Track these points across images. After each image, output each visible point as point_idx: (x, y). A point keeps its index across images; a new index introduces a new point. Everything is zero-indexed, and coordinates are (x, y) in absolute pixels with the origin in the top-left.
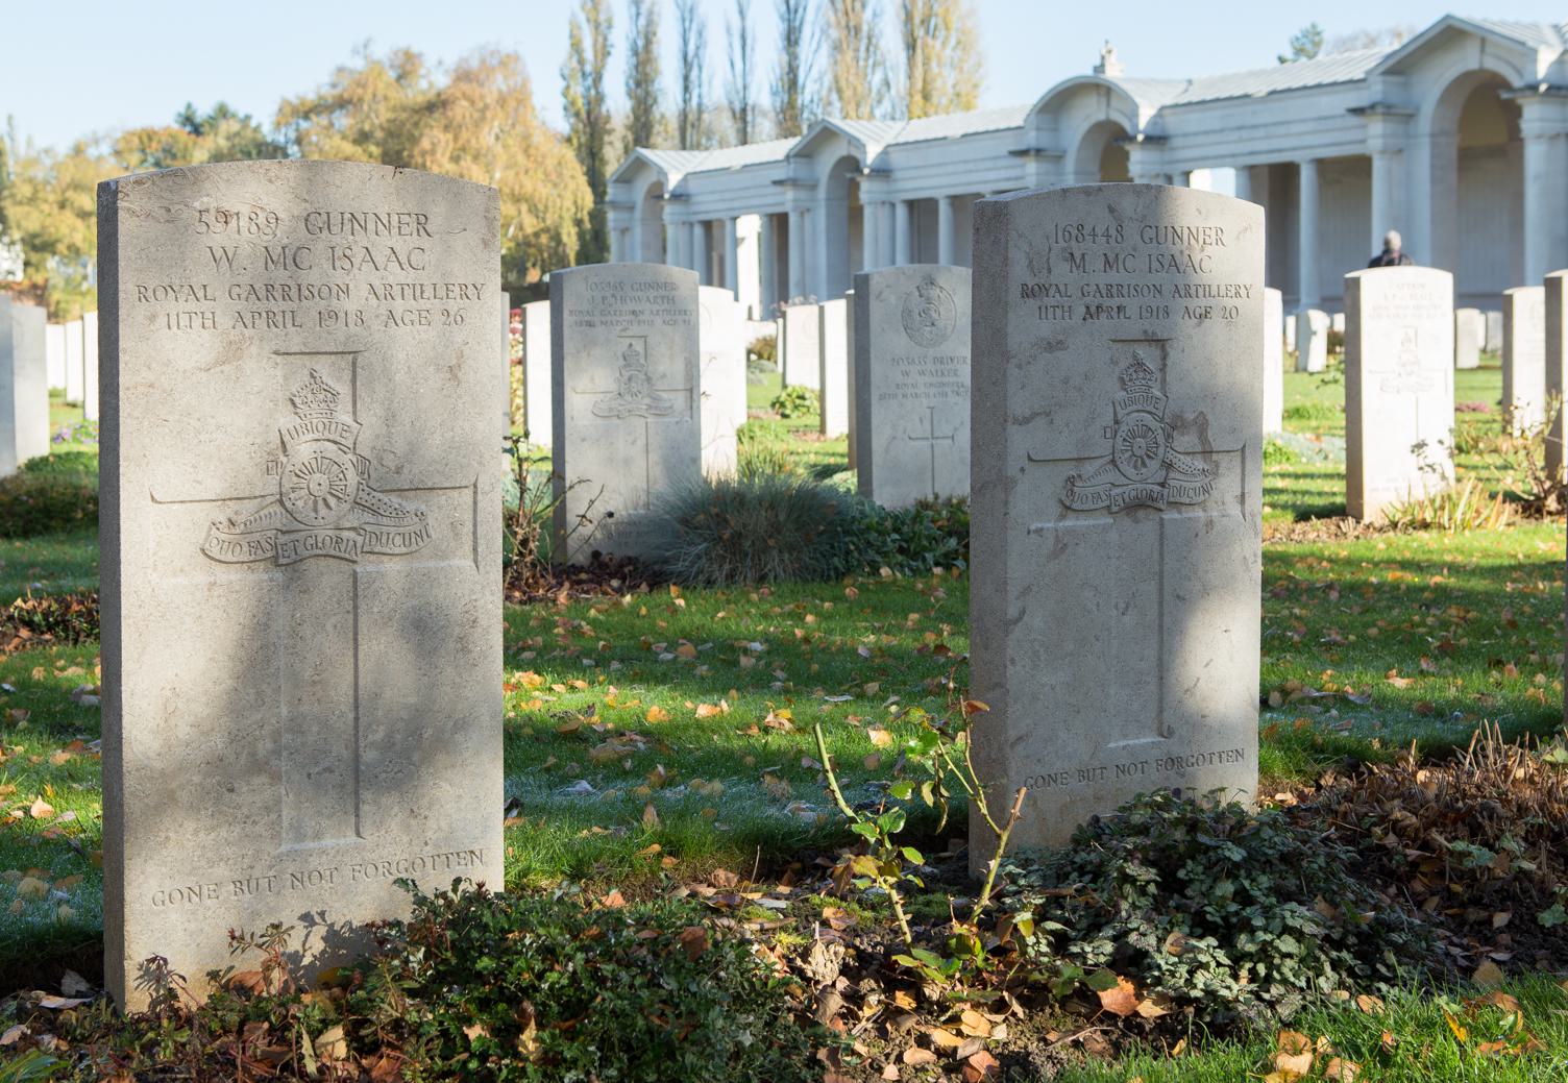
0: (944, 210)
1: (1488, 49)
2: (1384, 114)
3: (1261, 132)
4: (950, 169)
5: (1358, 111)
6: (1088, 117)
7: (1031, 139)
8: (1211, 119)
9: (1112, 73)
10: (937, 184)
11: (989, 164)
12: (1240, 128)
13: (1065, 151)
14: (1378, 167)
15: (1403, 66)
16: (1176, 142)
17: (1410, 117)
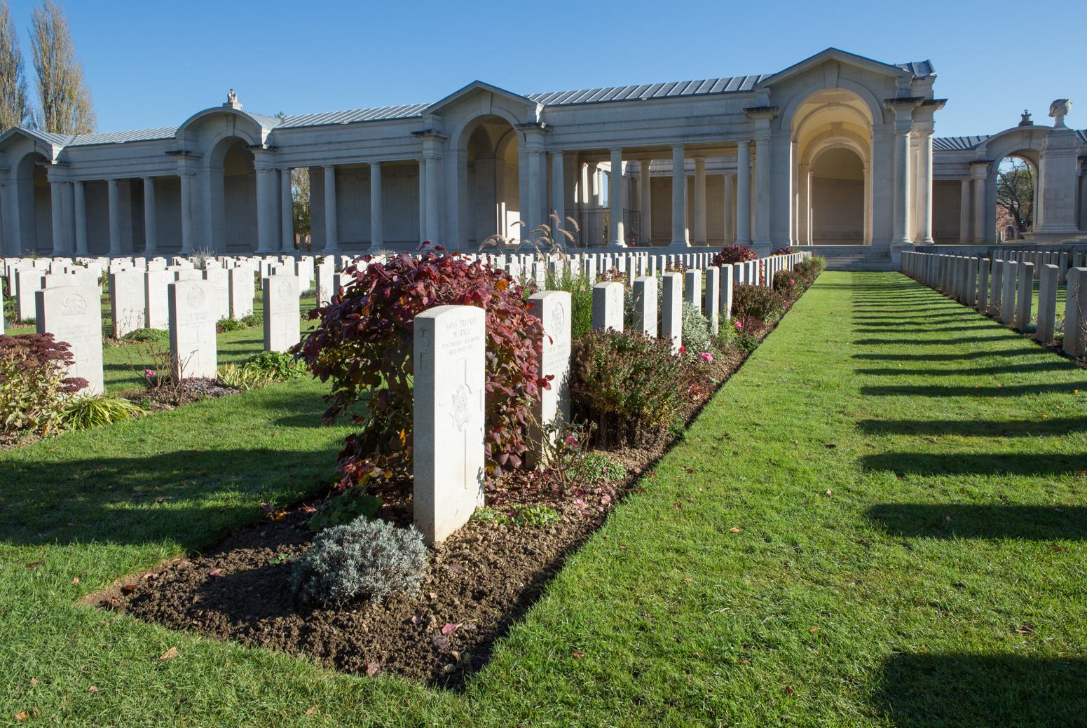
0: (375, 173)
1: (37, 144)
2: (185, 155)
3: (345, 146)
4: (117, 162)
5: (417, 134)
6: (220, 134)
7: (181, 145)
8: (309, 137)
9: (237, 106)
10: (109, 172)
11: (147, 160)
12: (329, 143)
13: (10, 167)
14: (184, 181)
15: (443, 110)
16: (285, 150)
17: (199, 158)
